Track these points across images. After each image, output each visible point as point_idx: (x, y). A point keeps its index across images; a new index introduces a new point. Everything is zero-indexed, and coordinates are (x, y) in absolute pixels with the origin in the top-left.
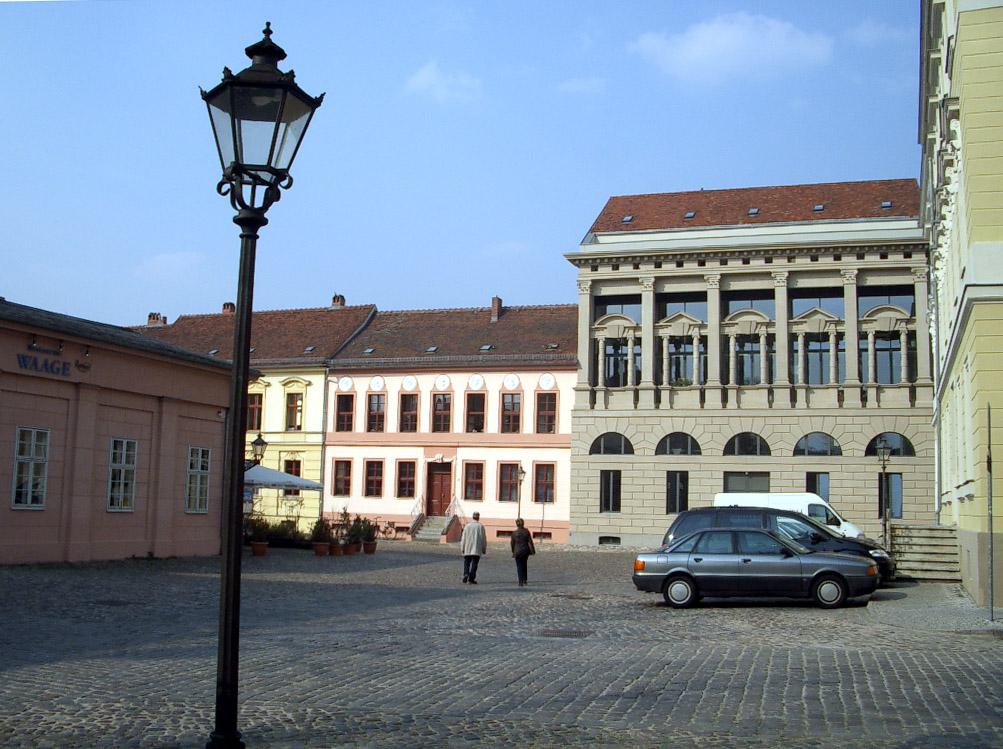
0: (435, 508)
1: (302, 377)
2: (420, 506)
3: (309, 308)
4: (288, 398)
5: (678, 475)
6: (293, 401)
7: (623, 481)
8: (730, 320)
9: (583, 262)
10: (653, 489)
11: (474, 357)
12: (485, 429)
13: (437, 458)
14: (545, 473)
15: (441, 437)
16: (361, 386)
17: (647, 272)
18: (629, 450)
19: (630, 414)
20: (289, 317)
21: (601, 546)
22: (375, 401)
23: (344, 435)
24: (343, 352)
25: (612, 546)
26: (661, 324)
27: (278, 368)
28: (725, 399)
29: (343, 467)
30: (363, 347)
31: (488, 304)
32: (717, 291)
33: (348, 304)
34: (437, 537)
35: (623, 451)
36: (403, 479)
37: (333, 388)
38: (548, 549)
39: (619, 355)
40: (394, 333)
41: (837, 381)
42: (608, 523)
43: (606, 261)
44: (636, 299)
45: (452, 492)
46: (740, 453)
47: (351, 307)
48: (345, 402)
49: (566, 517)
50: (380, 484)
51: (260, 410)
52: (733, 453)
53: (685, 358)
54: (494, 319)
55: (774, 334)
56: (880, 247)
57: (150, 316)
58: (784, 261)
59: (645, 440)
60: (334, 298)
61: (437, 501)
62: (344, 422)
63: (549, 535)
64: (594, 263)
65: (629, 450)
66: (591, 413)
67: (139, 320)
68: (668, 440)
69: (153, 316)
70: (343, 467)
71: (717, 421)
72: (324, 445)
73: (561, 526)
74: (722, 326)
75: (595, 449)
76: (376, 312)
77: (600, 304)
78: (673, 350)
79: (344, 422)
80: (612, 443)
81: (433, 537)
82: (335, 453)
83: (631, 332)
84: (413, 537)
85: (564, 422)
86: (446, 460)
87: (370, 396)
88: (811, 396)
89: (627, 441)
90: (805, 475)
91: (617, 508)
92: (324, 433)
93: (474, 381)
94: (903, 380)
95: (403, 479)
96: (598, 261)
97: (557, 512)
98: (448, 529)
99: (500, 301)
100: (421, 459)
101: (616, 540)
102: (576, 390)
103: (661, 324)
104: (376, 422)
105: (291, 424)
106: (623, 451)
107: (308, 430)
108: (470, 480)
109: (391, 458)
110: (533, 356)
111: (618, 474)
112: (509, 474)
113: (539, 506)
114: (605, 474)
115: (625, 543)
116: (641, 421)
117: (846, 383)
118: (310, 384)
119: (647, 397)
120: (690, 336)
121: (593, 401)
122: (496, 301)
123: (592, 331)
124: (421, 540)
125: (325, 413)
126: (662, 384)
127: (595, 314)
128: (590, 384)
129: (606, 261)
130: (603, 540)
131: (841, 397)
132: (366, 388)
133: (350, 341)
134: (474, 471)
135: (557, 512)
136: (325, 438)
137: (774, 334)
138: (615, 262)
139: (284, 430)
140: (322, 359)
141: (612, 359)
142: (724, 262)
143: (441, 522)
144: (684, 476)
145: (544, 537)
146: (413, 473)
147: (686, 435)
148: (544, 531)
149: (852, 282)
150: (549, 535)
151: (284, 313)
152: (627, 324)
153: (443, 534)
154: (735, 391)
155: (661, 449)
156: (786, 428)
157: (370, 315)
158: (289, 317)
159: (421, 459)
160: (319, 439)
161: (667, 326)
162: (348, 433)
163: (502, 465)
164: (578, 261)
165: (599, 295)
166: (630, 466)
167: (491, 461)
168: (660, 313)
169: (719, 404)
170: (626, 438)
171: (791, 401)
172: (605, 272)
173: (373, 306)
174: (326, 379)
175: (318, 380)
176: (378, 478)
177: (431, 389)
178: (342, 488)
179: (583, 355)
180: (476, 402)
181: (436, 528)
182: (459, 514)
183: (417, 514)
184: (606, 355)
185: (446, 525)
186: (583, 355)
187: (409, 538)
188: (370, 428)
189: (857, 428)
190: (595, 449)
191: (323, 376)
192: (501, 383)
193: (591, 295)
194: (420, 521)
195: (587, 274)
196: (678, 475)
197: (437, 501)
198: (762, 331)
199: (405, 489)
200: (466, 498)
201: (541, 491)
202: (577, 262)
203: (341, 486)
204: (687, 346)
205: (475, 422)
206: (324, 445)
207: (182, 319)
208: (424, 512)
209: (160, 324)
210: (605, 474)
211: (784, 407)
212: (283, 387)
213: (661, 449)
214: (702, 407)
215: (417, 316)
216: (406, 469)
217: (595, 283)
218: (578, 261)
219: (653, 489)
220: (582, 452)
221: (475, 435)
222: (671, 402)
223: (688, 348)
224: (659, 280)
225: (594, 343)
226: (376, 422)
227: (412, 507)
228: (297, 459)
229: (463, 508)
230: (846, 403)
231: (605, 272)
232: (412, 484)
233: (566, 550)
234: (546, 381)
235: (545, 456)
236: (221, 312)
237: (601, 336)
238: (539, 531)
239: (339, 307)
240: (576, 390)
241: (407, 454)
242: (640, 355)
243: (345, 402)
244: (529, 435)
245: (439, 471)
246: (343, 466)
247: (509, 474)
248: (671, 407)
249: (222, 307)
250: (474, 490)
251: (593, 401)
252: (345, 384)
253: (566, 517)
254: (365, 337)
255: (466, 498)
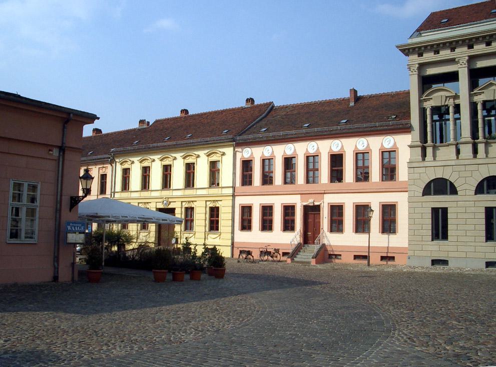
0: (309, 239)
1: (195, 153)
2: (298, 237)
3: (231, 108)
4: (163, 168)
5: (440, 210)
6: (214, 166)
7: (449, 216)
8: (426, 96)
9: (411, 50)
10: (474, 222)
11: (335, 127)
12: (253, 185)
13: (310, 202)
14: (389, 211)
15: (311, 187)
16: (256, 153)
17: (462, 53)
18: (454, 191)
19: (453, 163)
20: (218, 114)
21: (432, 267)
22: (361, 157)
23: (247, 188)
24: (247, 132)
25: (442, 267)
26: (475, 92)
27: (204, 144)
28: (475, 152)
29: (246, 211)
30: (261, 128)
31: (347, 95)
32: (466, 69)
33: (190, 113)
34: (308, 260)
35: (432, 192)
36: (287, 218)
37: (239, 156)
38: (390, 269)
39: (443, 120)
40: (283, 118)
41: (455, 138)
42: (438, 249)
43: (481, 39)
44: (453, 77)
45: (321, 227)
46: (435, 194)
47: (258, 105)
48: (247, 165)
49: (405, 244)
50: (271, 221)
51: (194, 173)
52: (482, 193)
53: (445, 124)
54: (352, 104)
55: (459, 105)
56: (484, 37)
57: (140, 122)
58: (465, 49)
59: (466, 182)
60: (247, 100)
61: (310, 233)
62: (247, 180)
63: (393, 258)
64: (419, 50)
65: (454, 191)
66: (422, 164)
67: (136, 125)
68: (432, 184)
69: (142, 122)
70: (246, 211)
71: (468, 168)
72: (234, 196)
73: (401, 251)
74: (471, 96)
75: (427, 191)
76: (273, 107)
77: (427, 82)
78: (485, 114)
79: (247, 180)
80: (440, 186)
81: (305, 260)
82: (241, 201)
83: (451, 100)
84: (292, 260)
85: (403, 173)
86: (316, 204)
87: (308, 157)
88: (489, 148)
89: (452, 184)
90: (484, 211)
91: (445, 237)
92: (234, 188)
93: (288, 149)
94: (452, 140)
95: (287, 218)
96: (423, 48)
97: (400, 240)
98: (317, 254)
99: (355, 92)
100: (298, 202)
101: (445, 262)
102: (411, 147)
103: (475, 92)
104: (363, 175)
105: (214, 181)
106: (432, 192)
107: (174, 188)
108: (334, 218)
109: (349, 202)
110: (377, 124)
111: (445, 211)
112: (362, 213)
113: (385, 236)
114: (435, 211)
115: (452, 265)
116: (463, 168)
117: (463, 140)
118: (224, 154)
119: (466, 150)
120: (447, 105)
121: (424, 155)
122: (353, 92)
123: (420, 102)
124: (298, 262)
125: (234, 173)
126: (478, 139)
127: (423, 88)
128: (421, 142)
129: (429, 48)
130: (435, 262)
131: (458, 152)
132: (304, 151)
133: (253, 125)
134: (337, 211)
135: (400, 240)
136: (234, 191)
137: (459, 105)
138: (436, 47)
139: (121, 191)
140: (231, 136)
141: (438, 123)
142: (471, 47)
143: (314, 248)
144: (445, 211)
145: (389, 260)
146: (293, 214)
147: (446, 180)
148: (390, 255)
149: (465, 66)
150: (393, 258)
151: (216, 112)
152: (448, 94)
153: (313, 258)
154: (484, 144)
155: (479, 190)
156: (468, 174)
157: (270, 108)
158: (218, 114)
159: (298, 202)
160: (230, 191)
161: (480, 94)
162: (249, 187)
163: (357, 206)
164: (407, 51)
165: (475, 67)
166: (454, 204)
167: (349, 202)
168: (473, 85)
169: (471, 155)
170: (450, 182)
171: (433, 156)
172: (429, 57)
173: (271, 103)
174: (234, 150)
175: (229, 151)
176: (292, 218)
177: (379, 147)
178: (246, 225)
179: (415, 120)
180: (337, 160)
181: (308, 254)
182: (326, 242)
183: (296, 243)
184: (433, 121)
185: (316, 250)
186: (415, 120)
187: (289, 261)
188: (358, 180)
189: (468, 174)
190: (427, 191)
191: (232, 148)
192: (355, 144)
193: (419, 75)
194: (298, 249)
195: (415, 59)
196: (440, 210)
197: (310, 233)
198: (451, 103)
199: (288, 226)
200: (331, 231)
201: (387, 226)
202: (407, 51)
203: (246, 224)
204: (446, 116)
205: (337, 174)
206: (234, 196)
207: (157, 121)
208: (302, 242)
209: (145, 126)
210: (435, 211)
211: (418, 161)
212: (183, 160)
213: (479, 190)
214: (458, 158)
215: (300, 107)
216: (289, 210)
217: (422, 66)
218: (407, 51)
219: (474, 222)
220: (417, 194)
221: (337, 185)
222: (487, 152)
223: (447, 116)
224: (472, 59)
225: (423, 111)
226: (363, 175)
227: (293, 238)
228: (217, 206)
229: (331, 239)
230: (461, 156)
231: (429, 57)
232: (293, 221)
233: (405, 270)
234: (389, 141)
235: (388, 198)
236: (179, 115)
237: (428, 105)
238: (385, 255)
239: (249, 106)
240: (411, 147)
241: (289, 200)
242: (459, 119)
243: (247, 165)
244: (350, 183)
245: (312, 211)
246: (246, 210)
247: (362, 213)
248: (487, 156)
249: (245, 102)
250: (337, 225)
251: (424, 155)
252: (246, 153)
253: (405, 244)
254: (263, 122)
255: (331, 231)
